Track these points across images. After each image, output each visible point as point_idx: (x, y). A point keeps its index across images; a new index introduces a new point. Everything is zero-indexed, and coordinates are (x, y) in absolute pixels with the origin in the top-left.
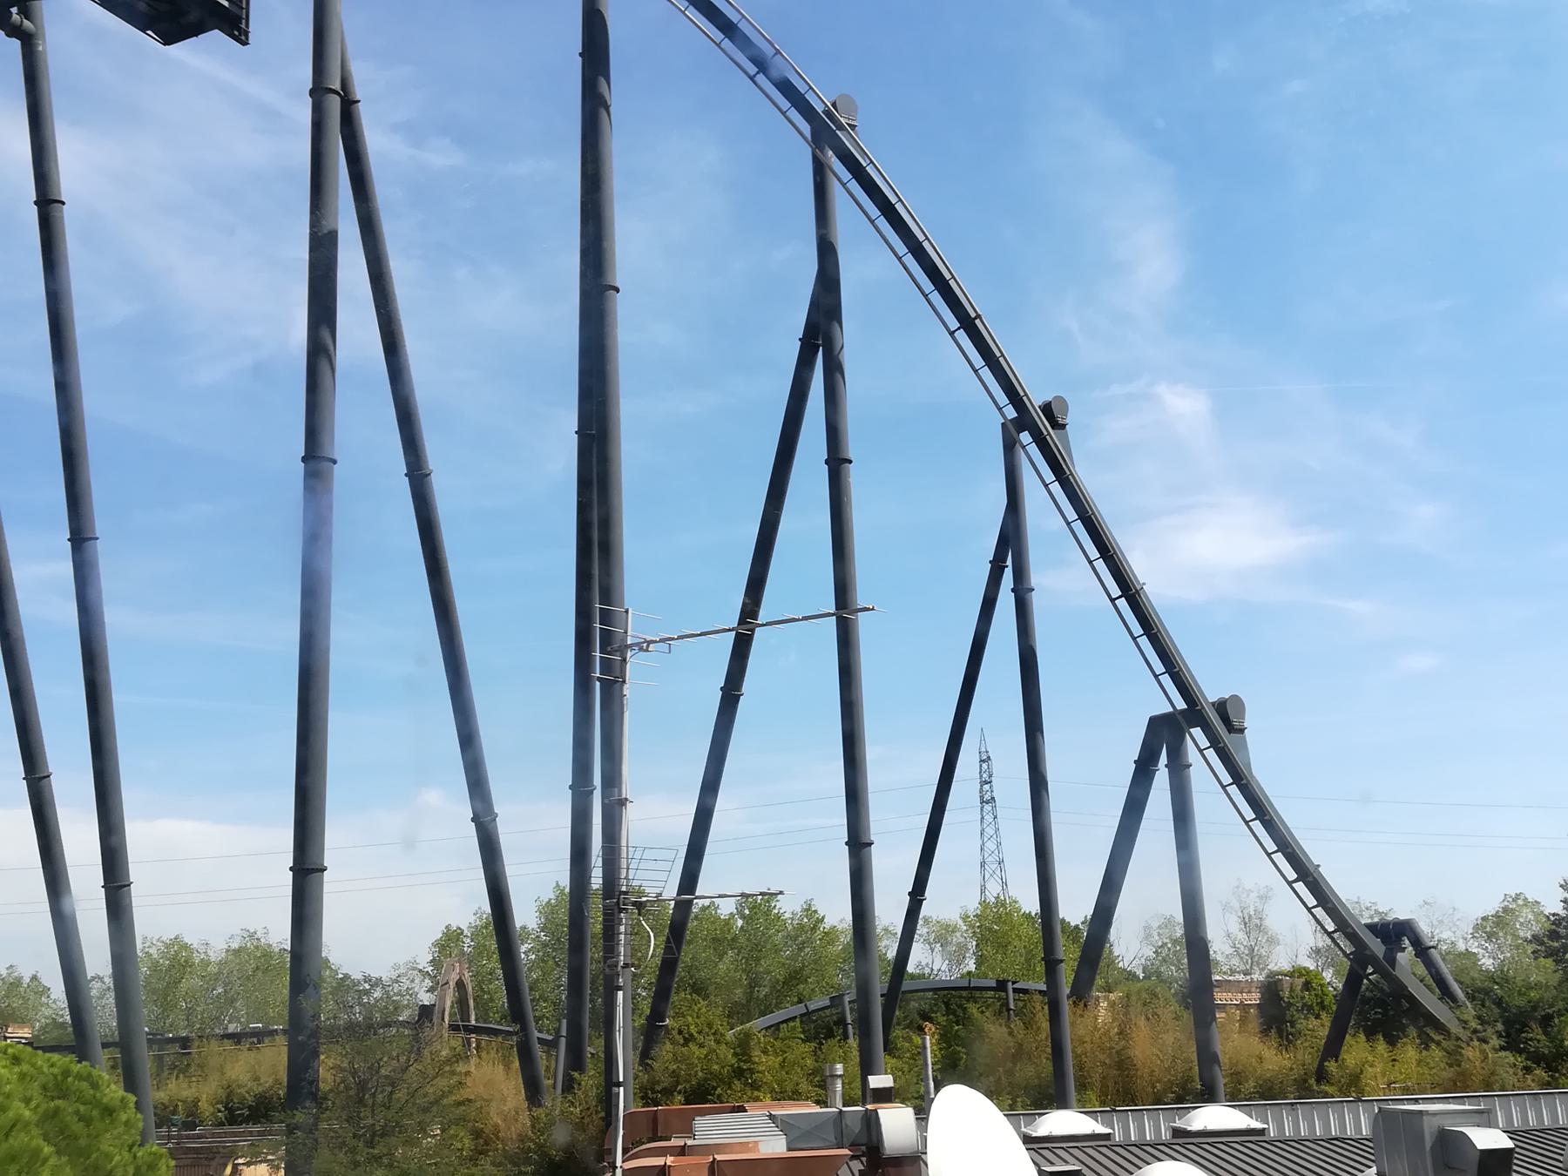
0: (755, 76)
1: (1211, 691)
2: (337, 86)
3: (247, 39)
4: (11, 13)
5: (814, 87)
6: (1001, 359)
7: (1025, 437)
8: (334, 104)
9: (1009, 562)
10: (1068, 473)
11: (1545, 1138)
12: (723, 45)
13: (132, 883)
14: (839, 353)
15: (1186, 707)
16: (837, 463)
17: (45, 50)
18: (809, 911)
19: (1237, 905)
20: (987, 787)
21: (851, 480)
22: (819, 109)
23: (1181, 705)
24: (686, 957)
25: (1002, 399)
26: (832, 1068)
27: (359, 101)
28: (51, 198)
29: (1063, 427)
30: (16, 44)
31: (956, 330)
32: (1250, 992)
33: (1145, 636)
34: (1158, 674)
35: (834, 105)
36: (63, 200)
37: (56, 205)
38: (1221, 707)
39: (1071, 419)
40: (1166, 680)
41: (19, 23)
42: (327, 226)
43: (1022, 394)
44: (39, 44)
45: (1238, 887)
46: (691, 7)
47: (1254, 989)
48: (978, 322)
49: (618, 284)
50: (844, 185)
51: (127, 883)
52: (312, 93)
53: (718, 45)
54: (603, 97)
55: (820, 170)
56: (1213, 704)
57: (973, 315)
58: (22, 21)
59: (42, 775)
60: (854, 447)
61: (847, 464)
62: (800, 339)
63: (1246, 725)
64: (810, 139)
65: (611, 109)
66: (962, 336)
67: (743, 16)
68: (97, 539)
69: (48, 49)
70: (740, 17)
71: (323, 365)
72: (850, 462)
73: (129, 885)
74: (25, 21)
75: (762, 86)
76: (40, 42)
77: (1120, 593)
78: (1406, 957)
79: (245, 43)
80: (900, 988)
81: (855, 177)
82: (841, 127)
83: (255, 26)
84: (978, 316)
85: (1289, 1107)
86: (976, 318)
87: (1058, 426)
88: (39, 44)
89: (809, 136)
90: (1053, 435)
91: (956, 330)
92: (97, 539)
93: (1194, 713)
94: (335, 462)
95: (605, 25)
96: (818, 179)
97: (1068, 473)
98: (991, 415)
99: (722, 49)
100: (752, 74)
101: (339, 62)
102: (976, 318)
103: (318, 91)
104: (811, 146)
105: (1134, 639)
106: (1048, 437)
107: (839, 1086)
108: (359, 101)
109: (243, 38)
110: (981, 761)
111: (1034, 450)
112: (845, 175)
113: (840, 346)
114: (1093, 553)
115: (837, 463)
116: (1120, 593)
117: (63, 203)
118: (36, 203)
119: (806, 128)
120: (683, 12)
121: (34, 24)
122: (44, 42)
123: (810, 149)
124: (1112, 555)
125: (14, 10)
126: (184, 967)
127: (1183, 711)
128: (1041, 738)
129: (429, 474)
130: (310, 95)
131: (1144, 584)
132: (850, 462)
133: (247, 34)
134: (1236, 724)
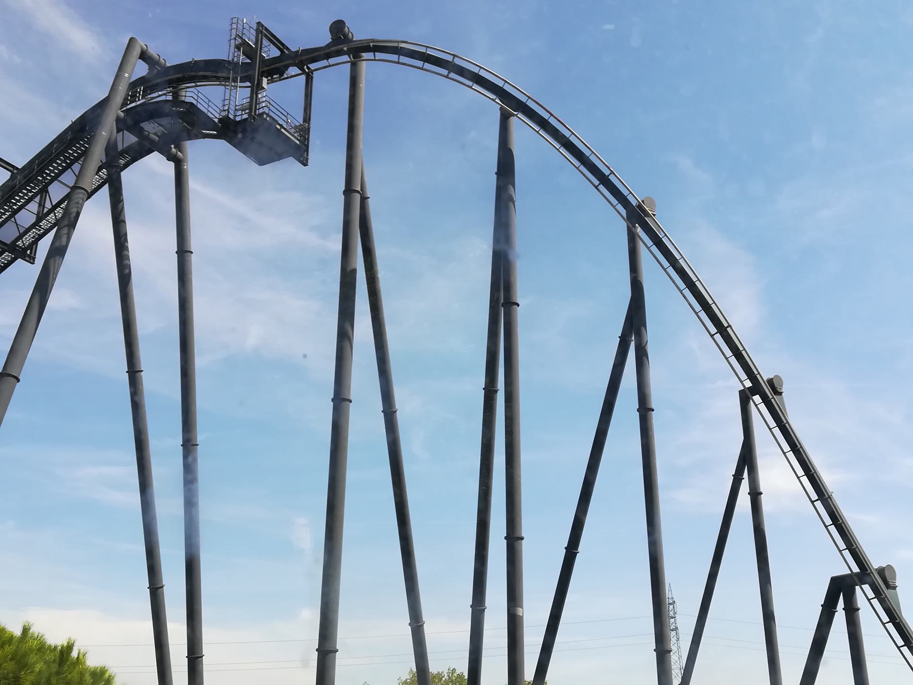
0: (598, 186)
1: (876, 562)
2: (359, 189)
4: (172, 148)
5: (667, 235)
6: (758, 376)
7: (757, 398)
8: (357, 197)
9: (746, 475)
10: (799, 447)
12: (580, 168)
13: (204, 655)
14: (645, 346)
15: (859, 571)
16: (644, 410)
17: (187, 168)
21: (653, 421)
22: (634, 203)
23: (856, 569)
25: (743, 376)
27: (369, 198)
28: (186, 249)
29: (781, 394)
30: (172, 165)
31: (715, 334)
33: (833, 526)
34: (827, 525)
35: (643, 202)
36: (192, 250)
37: (188, 253)
38: (881, 572)
39: (785, 389)
40: (847, 553)
41: (175, 153)
42: (350, 268)
43: (756, 373)
44: (185, 165)
46: (562, 147)
48: (729, 329)
49: (518, 302)
50: (648, 248)
51: (201, 655)
52: (345, 193)
53: (577, 168)
54: (512, 196)
55: (632, 239)
56: (876, 569)
57: (726, 325)
58: (177, 153)
59: (160, 586)
60: (655, 400)
61: (651, 412)
62: (619, 337)
64: (626, 218)
65: (515, 203)
66: (718, 337)
67: (593, 152)
68: (198, 445)
70: (591, 152)
71: (346, 344)
72: (653, 410)
73: (202, 657)
74: (179, 153)
75: (602, 191)
76: (185, 164)
77: (817, 498)
79: (305, 164)
81: (655, 244)
82: (647, 215)
83: (312, 156)
84: (729, 326)
86: (728, 327)
87: (778, 393)
88: (185, 165)
89: (625, 216)
90: (775, 400)
91: (715, 334)
92: (198, 445)
93: (864, 573)
94: (351, 401)
95: (513, 155)
96: (632, 245)
97: (799, 447)
98: (737, 382)
100: (446, 74)
101: (360, 176)
102: (728, 327)
103: (349, 191)
104: (626, 222)
105: (826, 527)
106: (787, 424)
108: (369, 198)
111: (763, 407)
112: (649, 243)
113: (646, 342)
114: (786, 448)
115: (644, 410)
116: (846, 547)
117: (192, 253)
118: (177, 252)
119: (624, 212)
121: (182, 153)
122: (187, 163)
123: (626, 224)
124: (841, 524)
125: (172, 146)
127: (857, 574)
128: (770, 587)
129: (396, 412)
130: (344, 195)
131: (832, 492)
132: (653, 410)
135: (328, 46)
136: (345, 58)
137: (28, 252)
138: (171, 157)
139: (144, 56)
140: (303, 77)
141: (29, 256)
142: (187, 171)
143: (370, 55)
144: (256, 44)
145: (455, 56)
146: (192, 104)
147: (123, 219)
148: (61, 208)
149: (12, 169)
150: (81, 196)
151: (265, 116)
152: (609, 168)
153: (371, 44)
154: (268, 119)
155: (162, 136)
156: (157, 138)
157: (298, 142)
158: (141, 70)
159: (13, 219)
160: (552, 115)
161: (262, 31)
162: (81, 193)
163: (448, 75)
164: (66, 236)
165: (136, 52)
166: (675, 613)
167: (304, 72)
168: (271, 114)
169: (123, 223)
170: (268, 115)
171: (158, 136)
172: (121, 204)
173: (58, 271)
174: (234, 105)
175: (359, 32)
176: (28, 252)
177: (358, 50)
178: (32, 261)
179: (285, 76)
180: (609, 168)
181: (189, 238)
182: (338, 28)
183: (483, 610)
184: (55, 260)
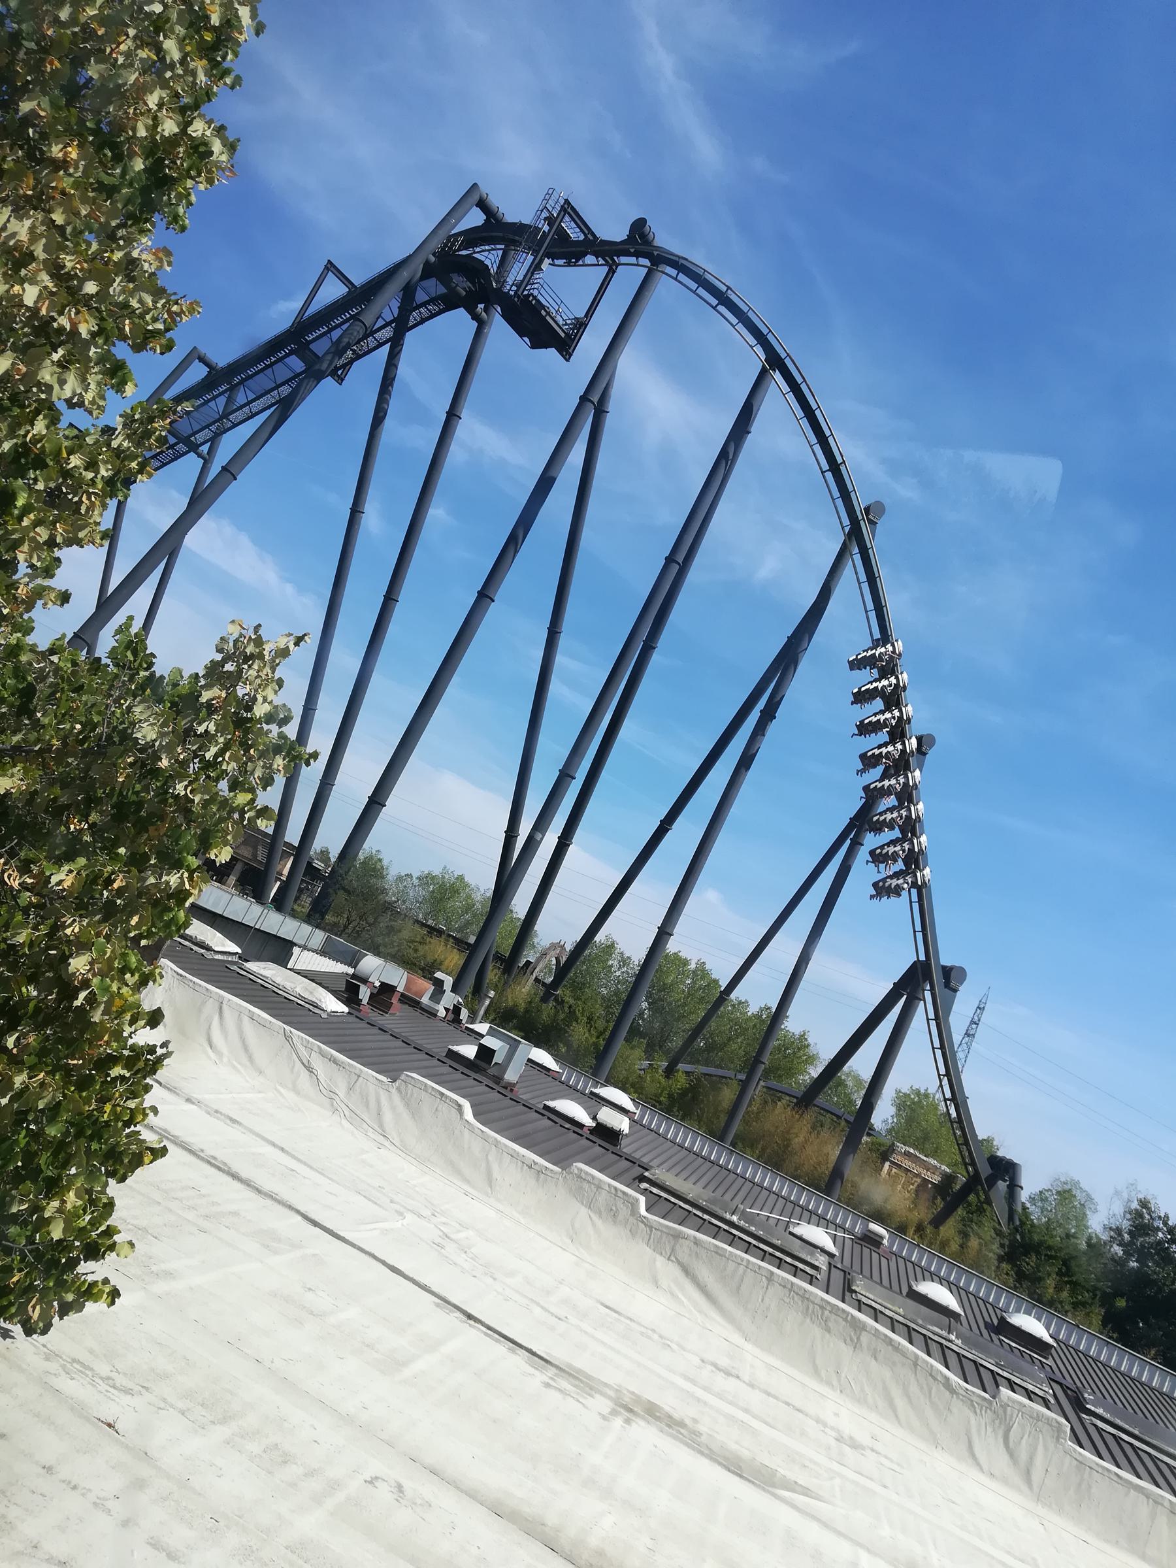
3: (570, 358)
11: (1158, 1406)
18: (802, 1037)
19: (1125, 1195)
20: (974, 1026)
24: (713, 1024)
26: (488, 992)
30: (475, 324)
32: (934, 1173)
42: (552, 473)
45: (1132, 1185)
47: (938, 1174)
63: (960, 989)
69: (490, 335)
78: (1002, 1185)
79: (567, 360)
80: (813, 1100)
85: (729, 1151)
94: (493, 601)
99: (812, 449)
107: (487, 1002)
109: (567, 357)
110: (978, 1007)
120: (798, 420)
126: (455, 892)
133: (571, 355)
134: (953, 985)
135: (623, 242)
136: (646, 262)
137: (340, 372)
138: (475, 317)
139: (483, 205)
140: (606, 269)
141: (338, 376)
142: (487, 337)
143: (673, 272)
144: (558, 215)
145: (729, 288)
146: (487, 266)
147: (396, 363)
148: (375, 338)
149: (350, 286)
150: (358, 328)
151: (531, 298)
152: (842, 456)
153: (655, 253)
154: (534, 302)
155: (470, 292)
156: (464, 293)
157: (563, 335)
158: (475, 218)
159: (329, 335)
160: (805, 380)
161: (568, 208)
162: (358, 325)
163: (716, 306)
164: (328, 362)
165: (476, 198)
166: (979, 1020)
167: (607, 263)
168: (540, 297)
169: (393, 367)
170: (535, 298)
171: (466, 291)
172: (400, 347)
173: (304, 399)
174: (513, 279)
175: (664, 239)
176: (340, 372)
177: (659, 259)
178: (340, 381)
179: (580, 262)
180: (842, 456)
181: (462, 402)
182: (639, 226)
183: (668, 830)
184: (309, 382)
